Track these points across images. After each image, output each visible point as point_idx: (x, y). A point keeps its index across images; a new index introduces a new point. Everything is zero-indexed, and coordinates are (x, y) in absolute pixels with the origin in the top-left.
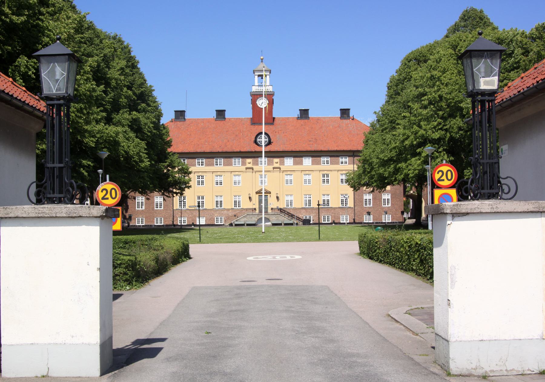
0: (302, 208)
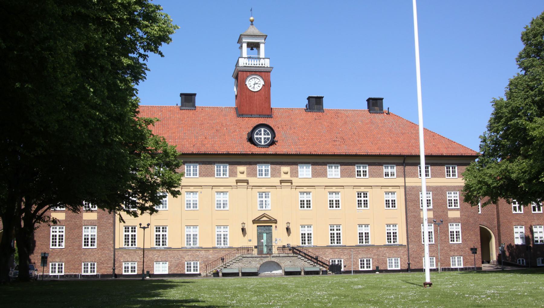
0: (328, 246)
